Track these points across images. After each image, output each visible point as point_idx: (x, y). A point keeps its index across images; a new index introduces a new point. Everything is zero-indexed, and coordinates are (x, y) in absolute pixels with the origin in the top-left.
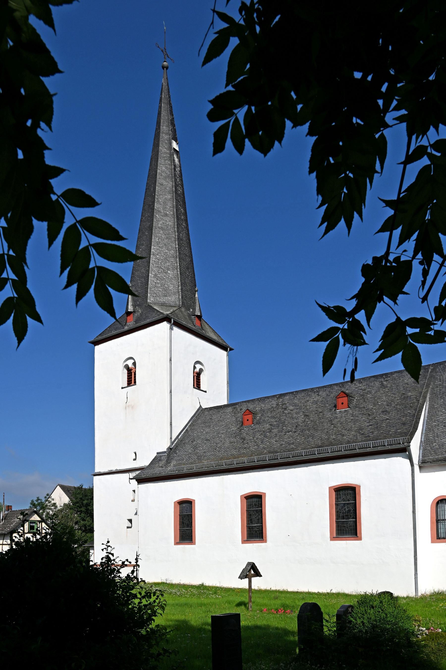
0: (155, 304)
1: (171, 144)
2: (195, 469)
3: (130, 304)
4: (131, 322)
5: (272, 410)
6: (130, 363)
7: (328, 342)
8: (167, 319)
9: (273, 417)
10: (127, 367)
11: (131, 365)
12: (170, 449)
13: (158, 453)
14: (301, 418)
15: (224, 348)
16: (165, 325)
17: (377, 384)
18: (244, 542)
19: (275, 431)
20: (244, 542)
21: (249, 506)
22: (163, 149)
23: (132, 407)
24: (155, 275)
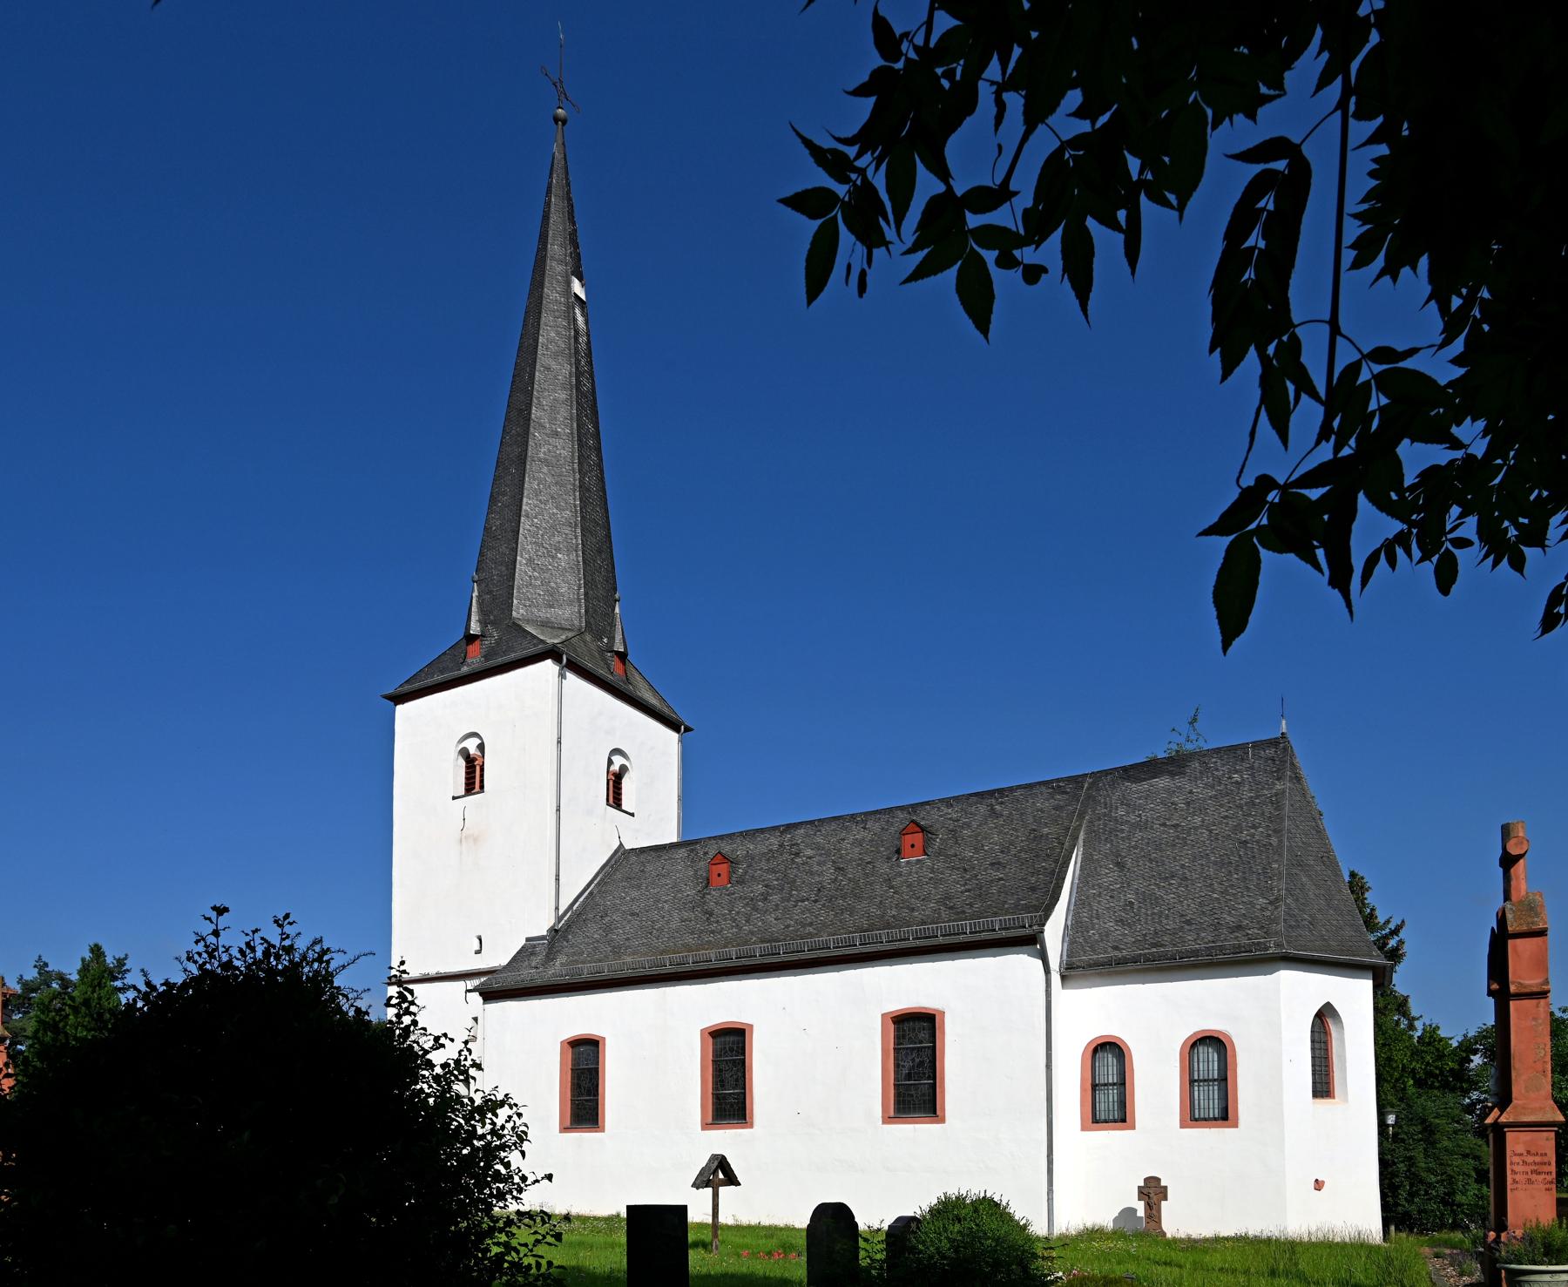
0: (528, 621)
1: (568, 284)
2: (606, 971)
3: (474, 618)
5: (769, 855)
6: (472, 745)
8: (553, 654)
10: (465, 753)
11: (473, 751)
13: (528, 939)
14: (829, 872)
15: (673, 725)
16: (548, 667)
17: (983, 809)
19: (776, 898)
20: (706, 1126)
22: (552, 294)
24: (530, 561)
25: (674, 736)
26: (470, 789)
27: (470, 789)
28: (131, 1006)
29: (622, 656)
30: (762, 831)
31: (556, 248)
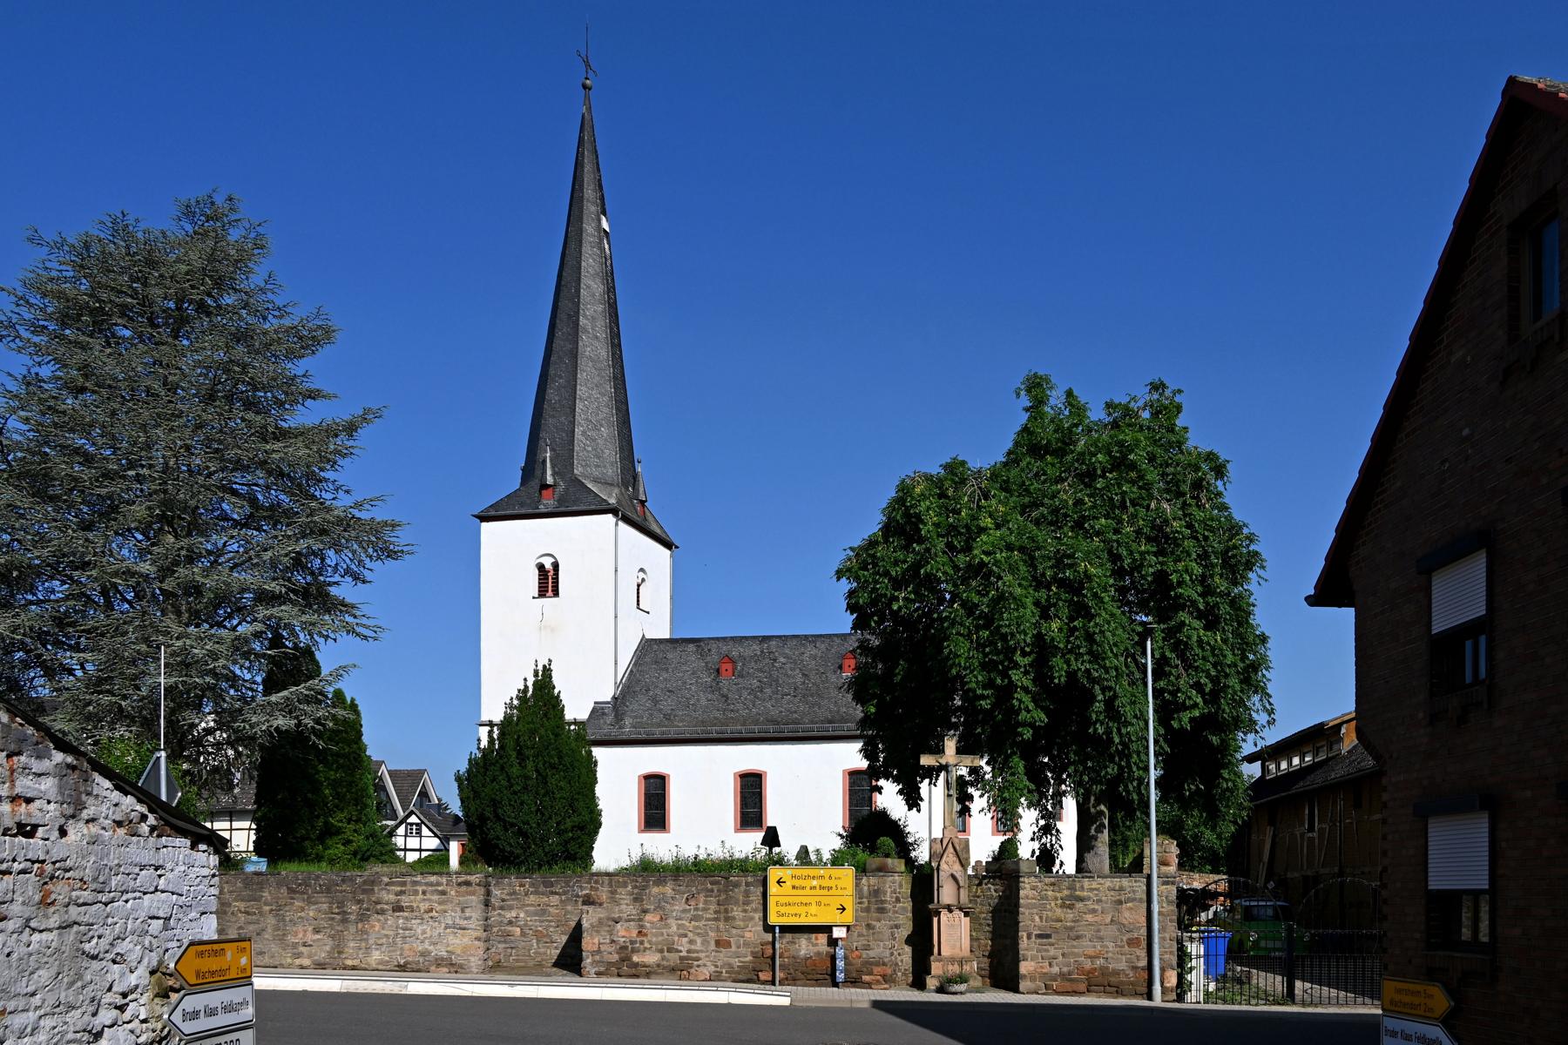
0: (586, 477)
1: (599, 221)
2: (657, 733)
3: (549, 472)
4: (548, 503)
5: (756, 659)
6: (548, 563)
7: (1264, 994)
8: (613, 511)
9: (761, 670)
10: (541, 567)
11: (548, 566)
12: (614, 698)
14: (799, 679)
15: (668, 545)
16: (610, 518)
18: (737, 831)
19: (768, 691)
20: (737, 831)
21: (743, 787)
22: (589, 228)
23: (553, 630)
24: (584, 433)
25: (668, 552)
26: (542, 593)
27: (542, 593)
28: (939, 751)
29: (643, 503)
30: (746, 638)
31: (589, 192)
